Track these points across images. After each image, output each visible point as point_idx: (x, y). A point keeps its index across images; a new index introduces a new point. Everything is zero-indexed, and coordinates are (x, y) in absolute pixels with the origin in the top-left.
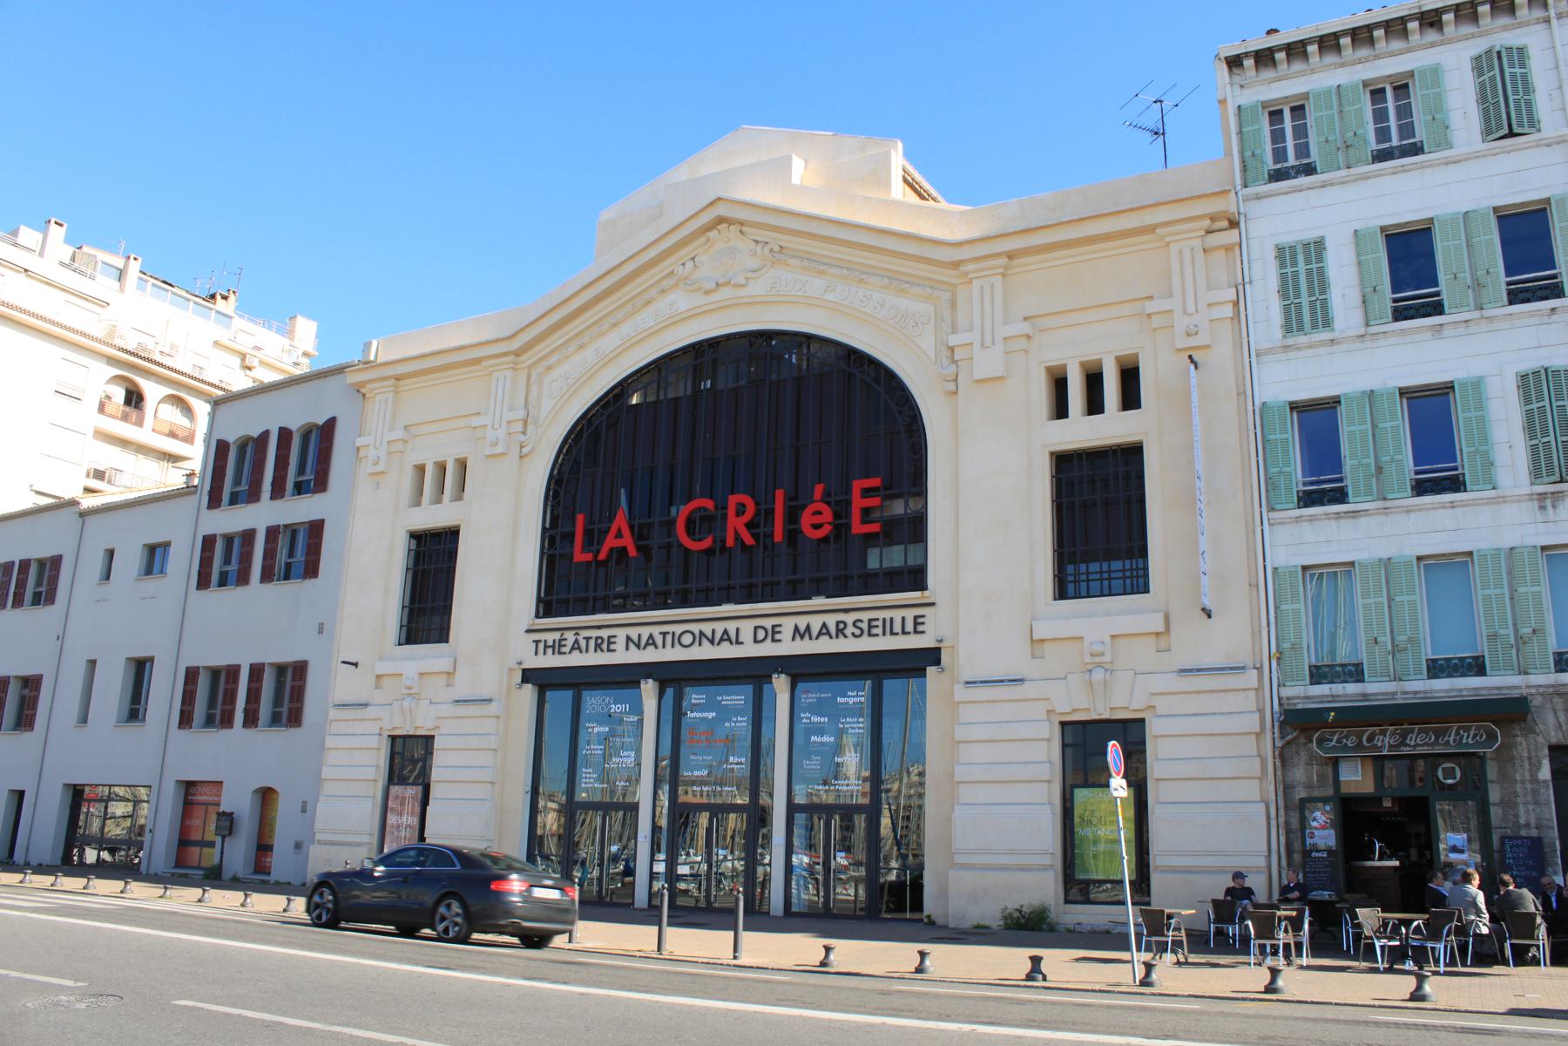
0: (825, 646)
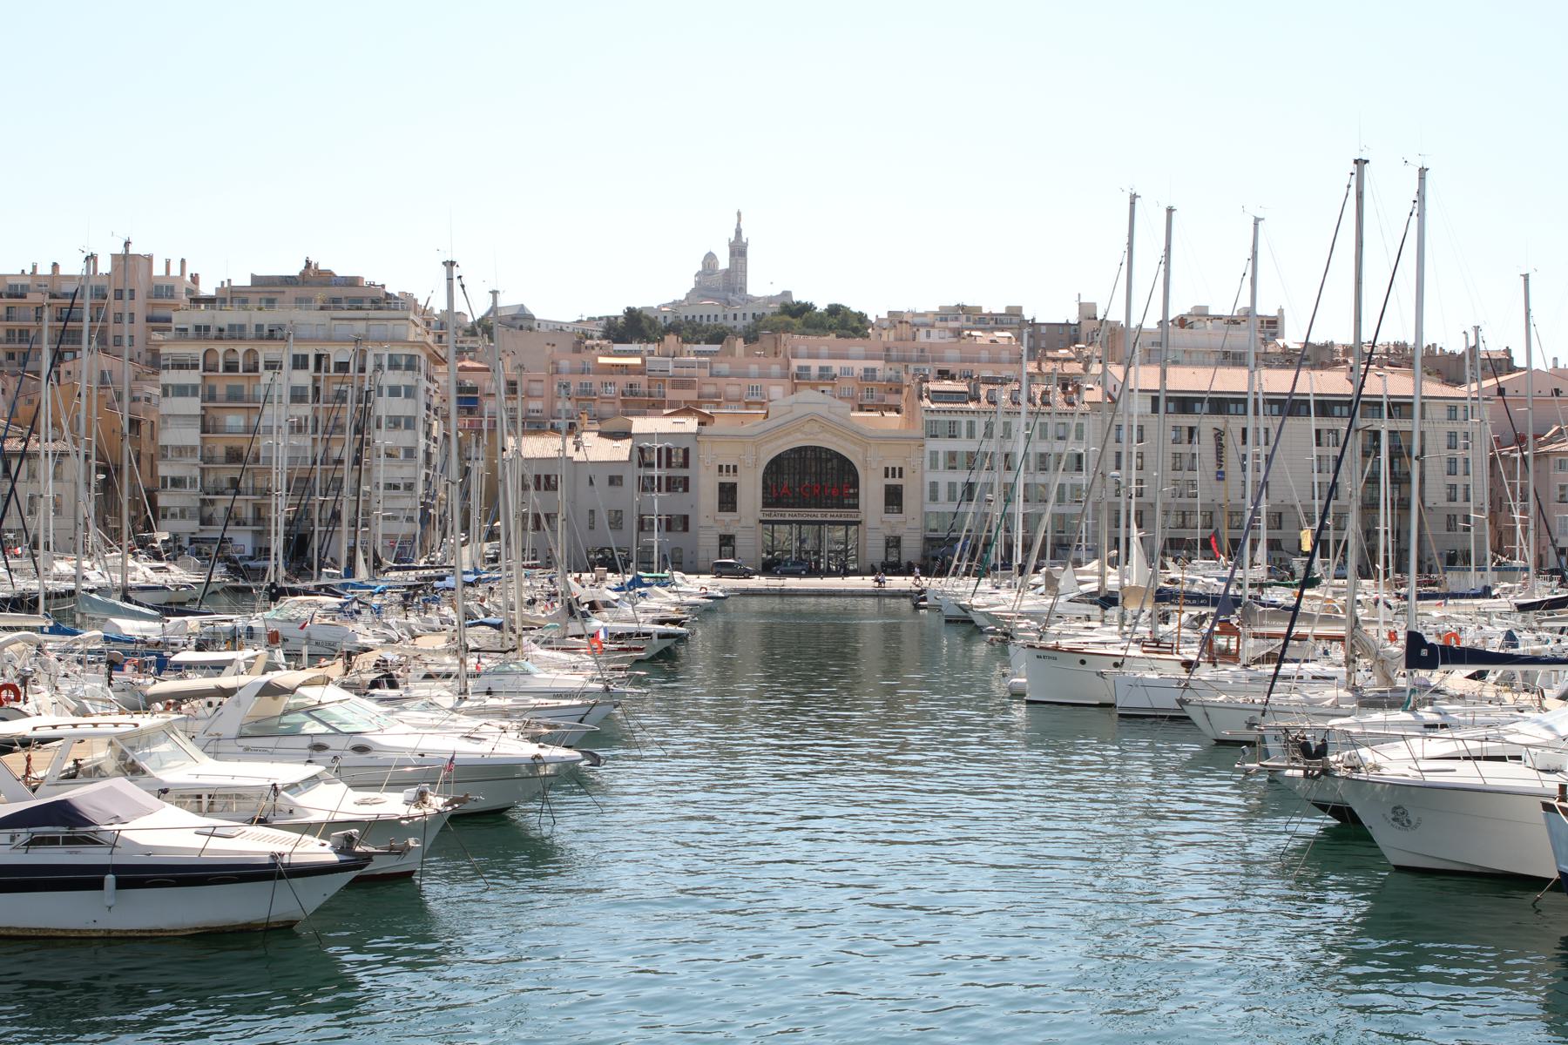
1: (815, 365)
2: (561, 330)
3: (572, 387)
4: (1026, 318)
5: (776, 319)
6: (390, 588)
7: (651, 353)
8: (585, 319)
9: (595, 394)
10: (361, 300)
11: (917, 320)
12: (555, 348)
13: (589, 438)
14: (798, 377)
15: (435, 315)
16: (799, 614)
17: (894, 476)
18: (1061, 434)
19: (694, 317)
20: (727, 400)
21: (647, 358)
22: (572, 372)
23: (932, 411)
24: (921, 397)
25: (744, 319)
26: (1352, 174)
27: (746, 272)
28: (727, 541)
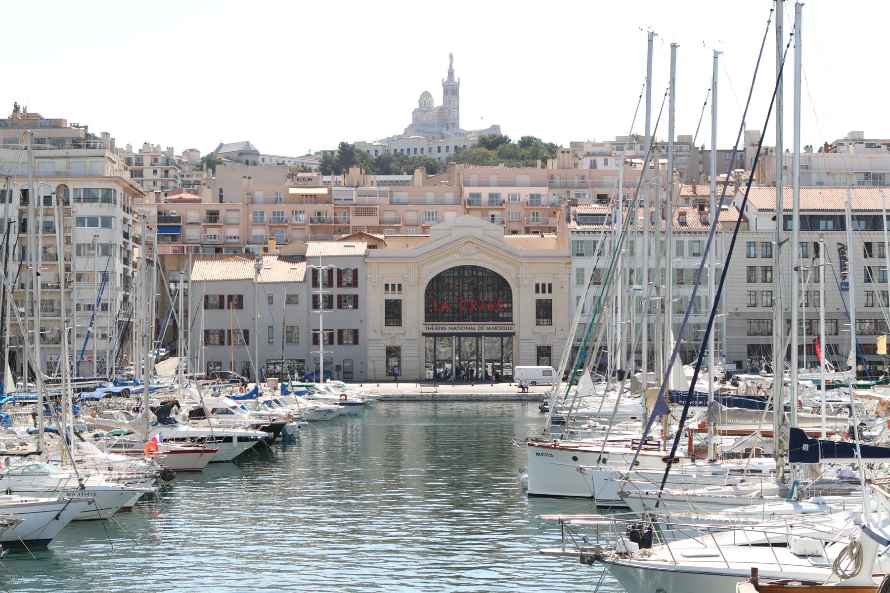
0: (493, 331)
1: (485, 192)
2: (283, 163)
3: (266, 216)
4: (696, 145)
5: (474, 151)
6: (20, 399)
7: (338, 184)
8: (313, 153)
9: (286, 222)
10: (62, 140)
11: (597, 150)
12: (251, 181)
13: (270, 261)
14: (470, 203)
15: (162, 153)
16: (477, 416)
17: (544, 292)
18: (696, 251)
19: (402, 150)
20: (406, 225)
21: (333, 189)
22: (266, 202)
23: (578, 232)
24: (568, 220)
25: (447, 151)
26: (772, 10)
27: (458, 108)
28: (393, 352)
